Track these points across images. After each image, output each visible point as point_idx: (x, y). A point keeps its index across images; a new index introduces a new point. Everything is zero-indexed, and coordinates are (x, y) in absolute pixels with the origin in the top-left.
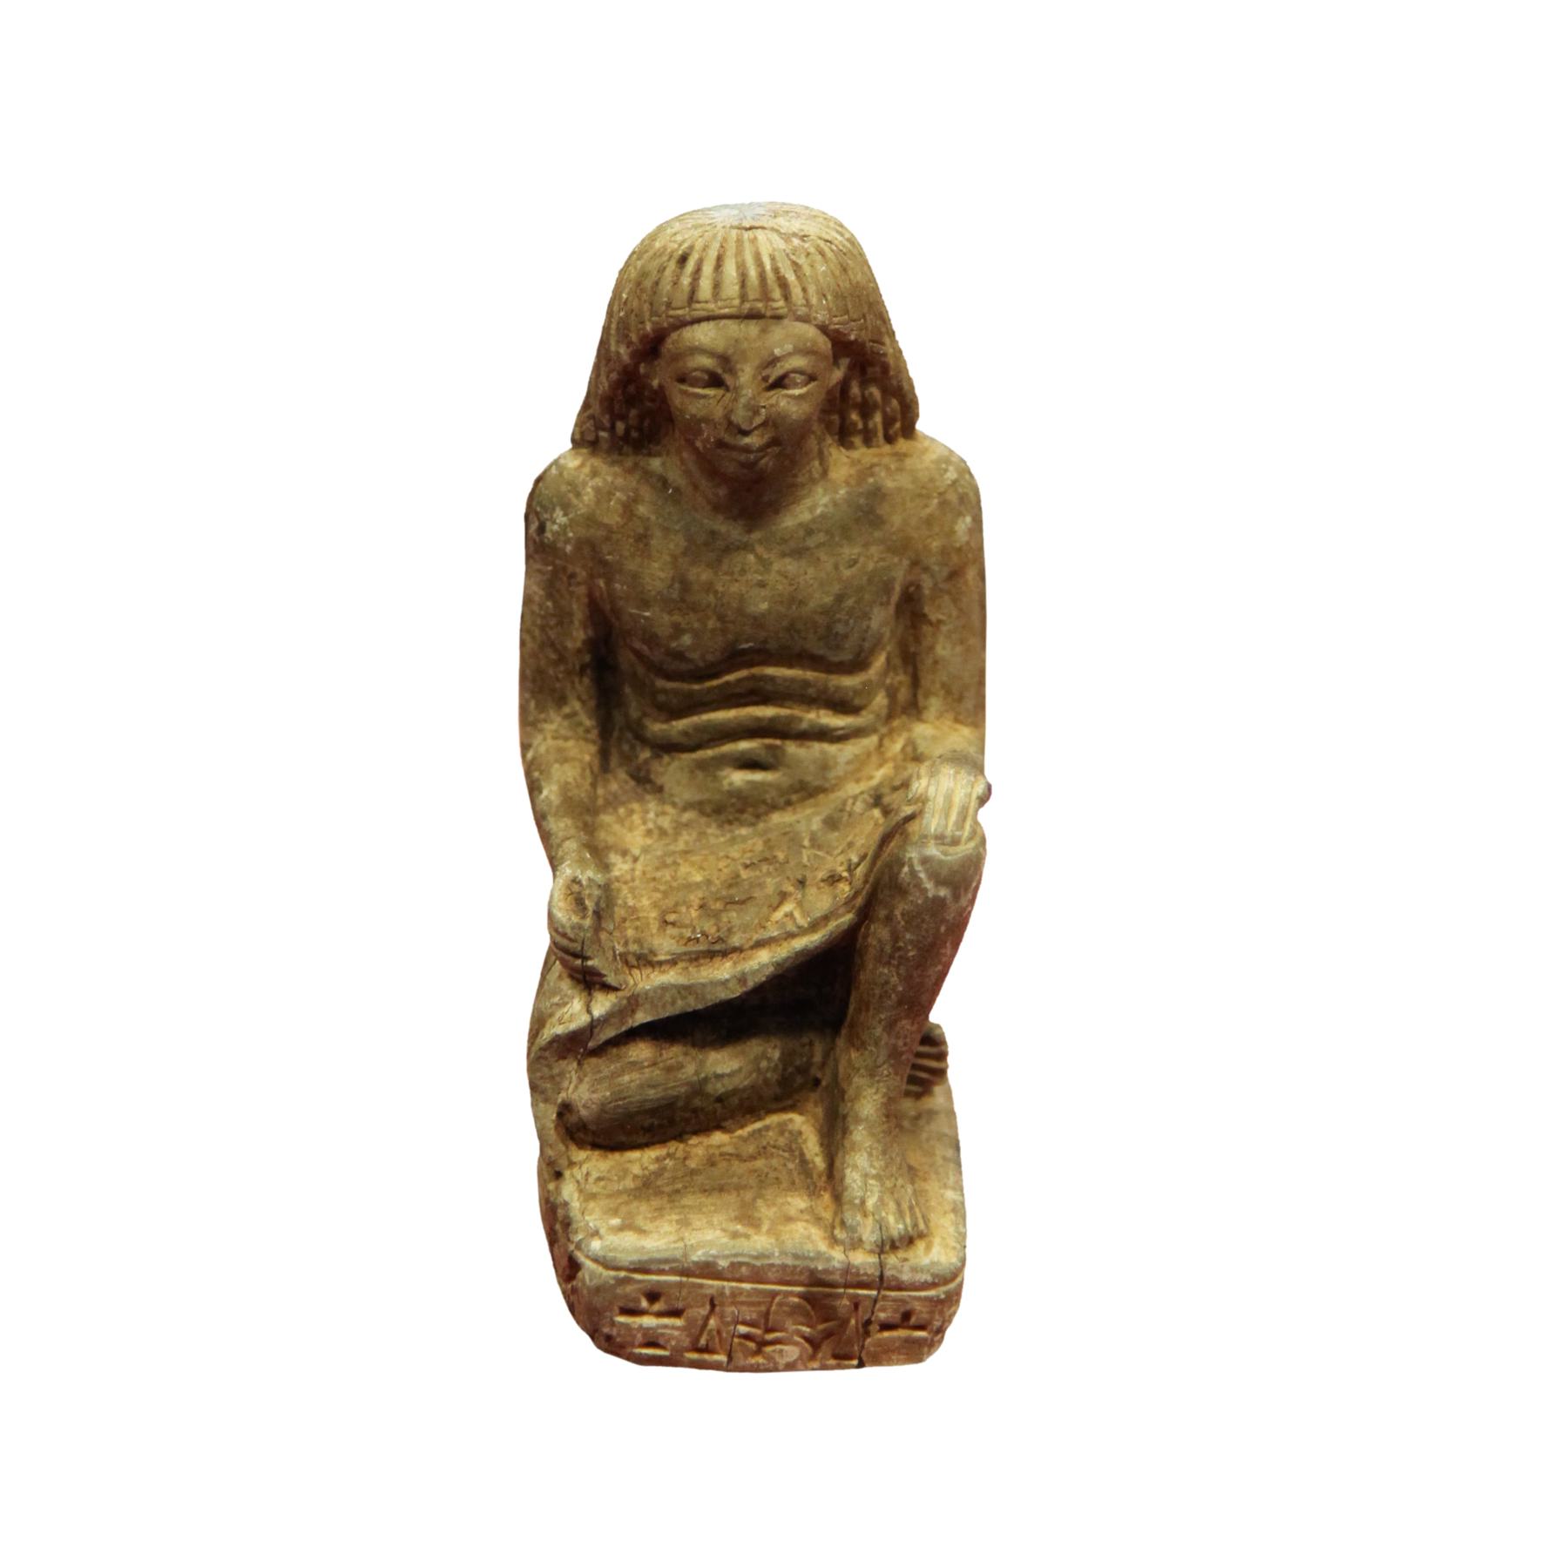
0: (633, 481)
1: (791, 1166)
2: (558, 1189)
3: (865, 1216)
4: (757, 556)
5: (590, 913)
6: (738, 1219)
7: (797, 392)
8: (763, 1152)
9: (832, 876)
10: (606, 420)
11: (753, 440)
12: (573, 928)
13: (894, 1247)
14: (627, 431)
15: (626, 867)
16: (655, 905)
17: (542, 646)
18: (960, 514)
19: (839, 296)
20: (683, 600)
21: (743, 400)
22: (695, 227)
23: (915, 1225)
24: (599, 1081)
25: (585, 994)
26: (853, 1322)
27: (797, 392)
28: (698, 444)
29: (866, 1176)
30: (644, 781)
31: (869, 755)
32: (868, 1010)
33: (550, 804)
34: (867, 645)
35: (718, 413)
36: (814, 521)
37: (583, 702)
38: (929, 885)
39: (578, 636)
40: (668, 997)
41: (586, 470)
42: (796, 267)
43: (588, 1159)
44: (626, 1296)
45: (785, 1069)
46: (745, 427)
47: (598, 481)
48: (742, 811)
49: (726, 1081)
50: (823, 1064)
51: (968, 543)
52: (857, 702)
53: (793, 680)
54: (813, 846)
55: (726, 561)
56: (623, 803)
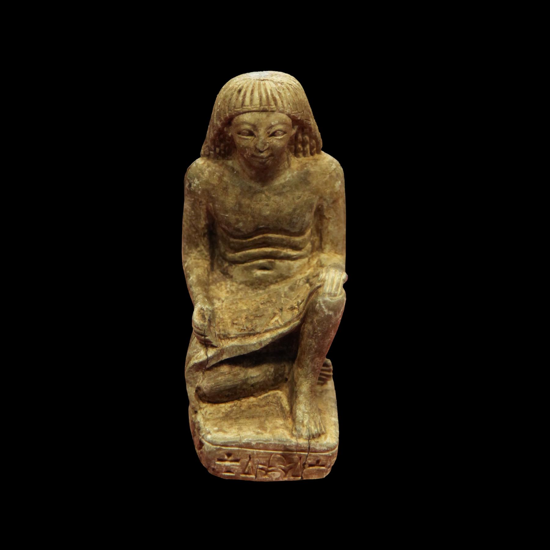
0: (222, 169)
1: (277, 409)
2: (196, 417)
3: (304, 426)
4: (265, 195)
5: (207, 320)
6: (259, 428)
7: (279, 137)
8: (268, 404)
9: (292, 307)
10: (212, 147)
11: (264, 154)
12: (201, 325)
13: (314, 437)
14: (220, 151)
15: (220, 304)
16: (230, 317)
17: (190, 227)
18: (337, 180)
19: (294, 104)
20: (240, 211)
21: (261, 140)
22: (244, 80)
23: (321, 430)
24: (210, 379)
25: (205, 349)
26: (299, 464)
27: (279, 137)
28: (245, 156)
29: (304, 412)
30: (226, 274)
31: (305, 265)
32: (304, 354)
33: (193, 282)
34: (304, 226)
35: (252, 145)
36: (285, 183)
37: (205, 246)
38: (326, 311)
39: (203, 223)
40: (234, 350)
41: (206, 165)
42: (279, 94)
43: (206, 406)
44: (220, 455)
45: (275, 375)
46: (261, 150)
47: (210, 169)
48: (260, 285)
49: (255, 379)
50: (289, 373)
51: (339, 190)
52: (301, 246)
53: (278, 239)
54: (285, 297)
55: (255, 197)
56: (219, 282)
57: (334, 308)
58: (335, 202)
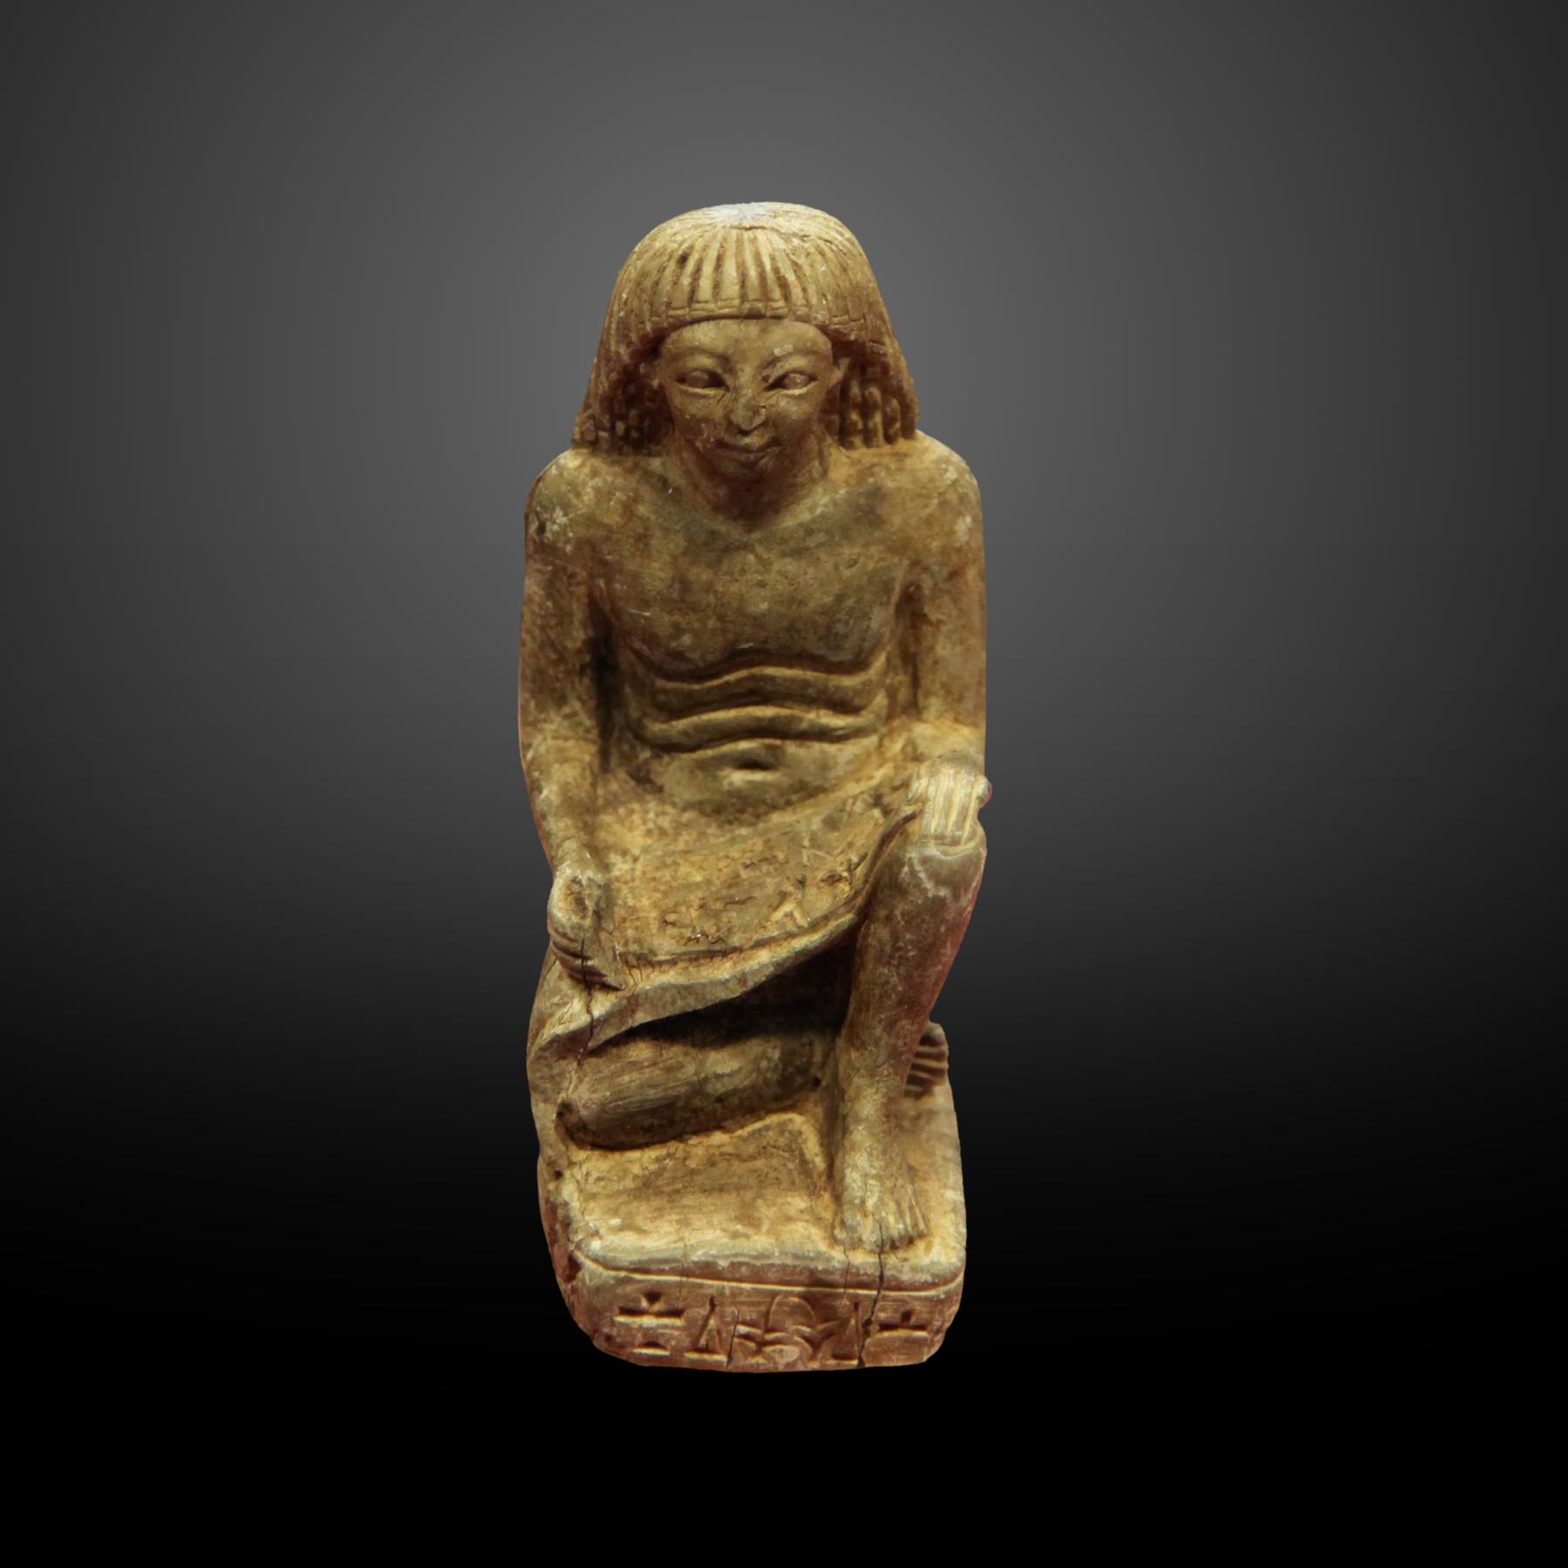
0: (633, 481)
1: (791, 1166)
2: (558, 1189)
3: (865, 1216)
4: (757, 556)
5: (590, 913)
6: (738, 1219)
7: (797, 392)
8: (763, 1152)
9: (832, 876)
10: (606, 420)
11: (753, 440)
12: (573, 928)
13: (894, 1247)
14: (627, 431)
15: (626, 867)
16: (655, 905)
17: (542, 646)
18: (960, 514)
19: (839, 296)
20: (683, 600)
21: (743, 400)
22: (695, 227)
23: (915, 1225)
24: (599, 1081)
25: (585, 994)
26: (853, 1322)
27: (797, 392)
28: (698, 444)
29: (866, 1176)
30: (644, 781)
31: (869, 755)
32: (868, 1010)
33: (550, 804)
34: (867, 645)
35: (718, 413)
36: (814, 521)
37: (583, 702)
38: (929, 885)
39: (578, 636)
40: (668, 997)
41: (586, 470)
42: (796, 267)
43: (588, 1159)
44: (626, 1296)
45: (785, 1069)
46: (745, 427)
47: (598, 481)
48: (742, 811)
49: (726, 1081)
50: (823, 1064)
51: (968, 543)
52: (857, 702)
53: (793, 680)
54: (813, 846)
55: (726, 561)
56: (623, 803)
57: (954, 880)
58: (955, 575)
